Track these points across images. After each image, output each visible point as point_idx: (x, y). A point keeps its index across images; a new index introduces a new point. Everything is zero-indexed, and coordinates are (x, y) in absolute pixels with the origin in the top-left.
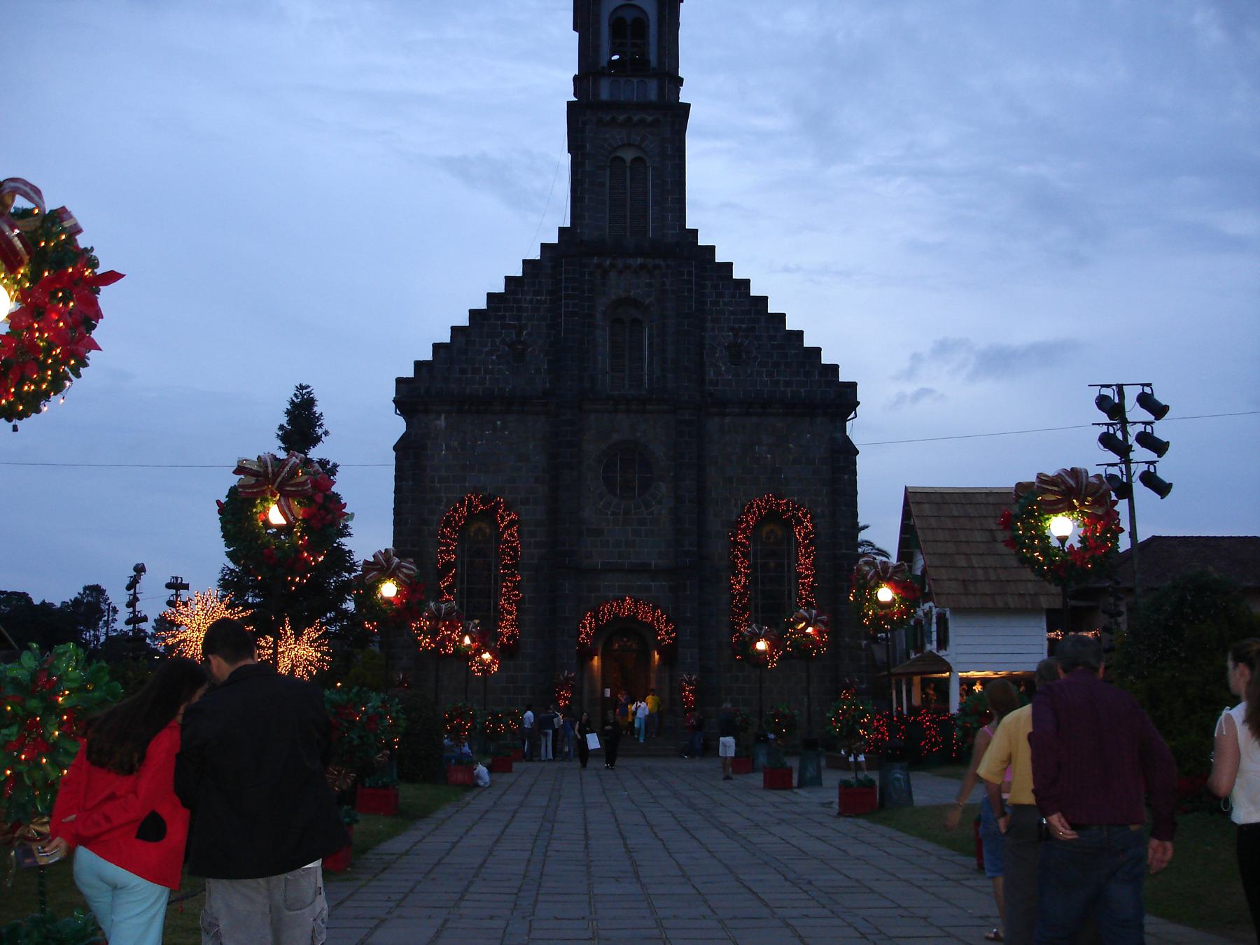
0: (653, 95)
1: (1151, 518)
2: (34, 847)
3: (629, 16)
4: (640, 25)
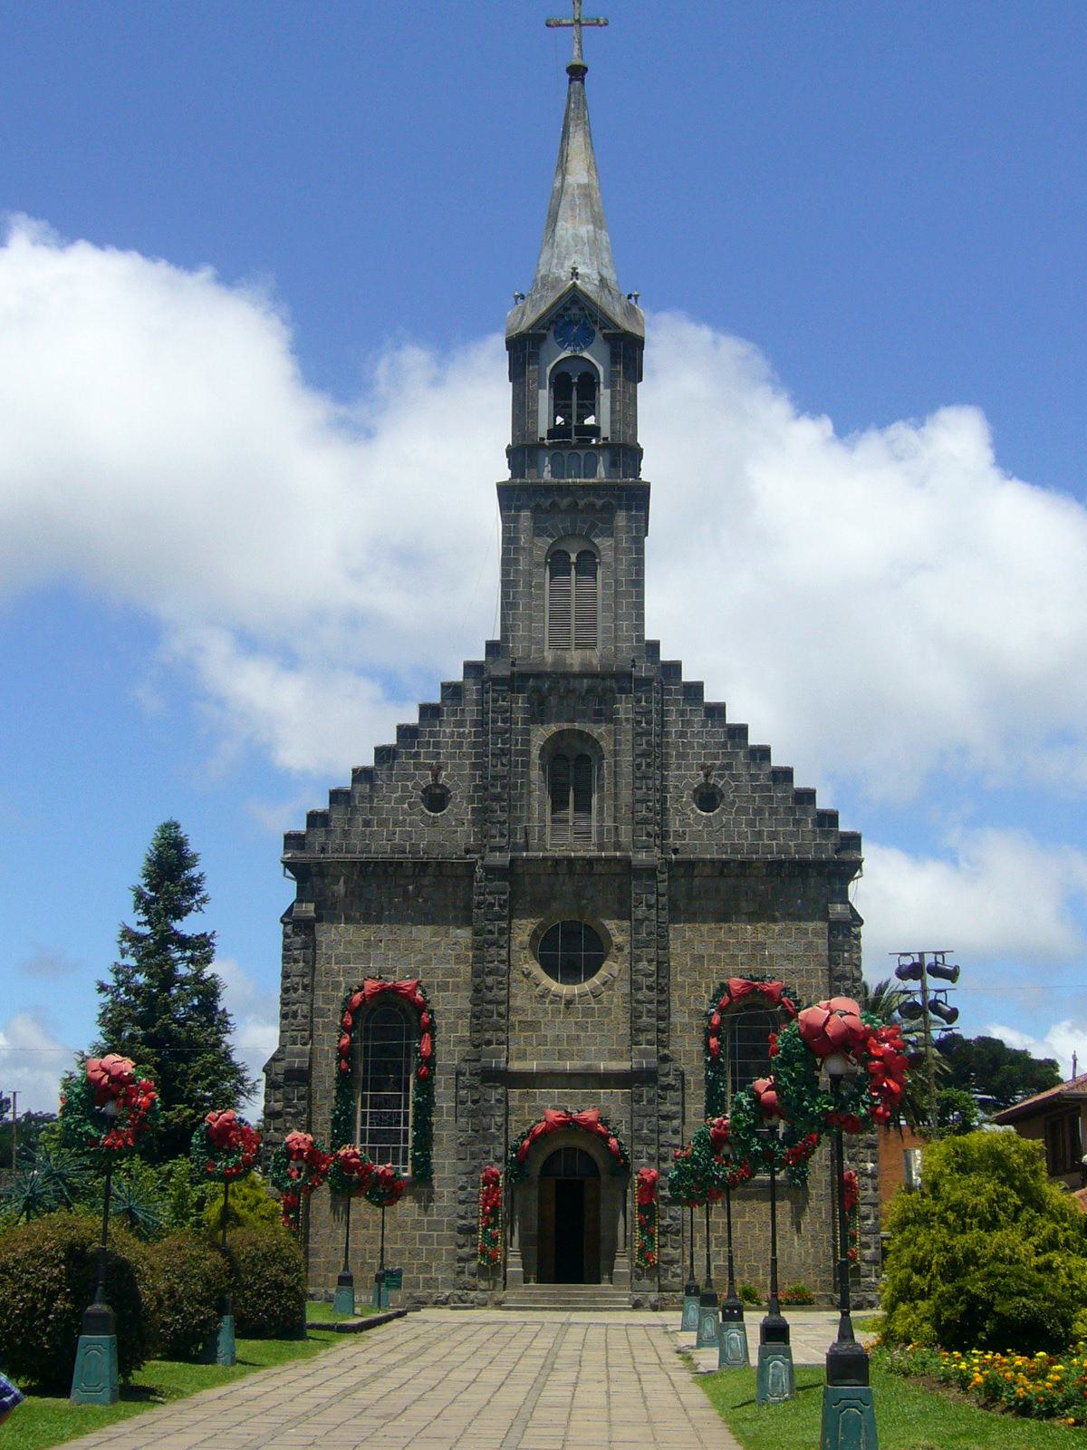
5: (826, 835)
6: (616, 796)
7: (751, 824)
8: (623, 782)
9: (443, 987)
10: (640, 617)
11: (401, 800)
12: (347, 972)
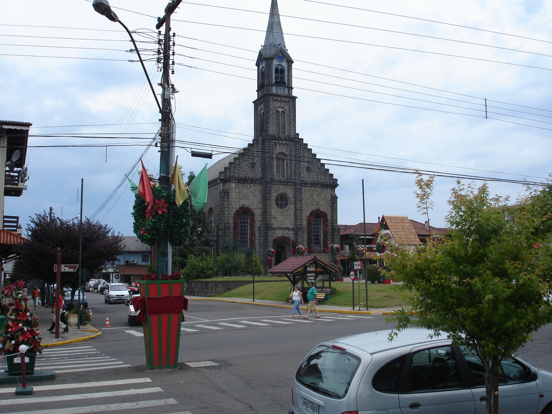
0: (287, 93)
1: (390, 331)
2: (448, 357)
3: (280, 68)
4: (282, 71)
5: (331, 179)
6: (291, 168)
7: (317, 176)
8: (293, 165)
9: (256, 209)
10: (295, 128)
11: (246, 166)
12: (235, 205)
